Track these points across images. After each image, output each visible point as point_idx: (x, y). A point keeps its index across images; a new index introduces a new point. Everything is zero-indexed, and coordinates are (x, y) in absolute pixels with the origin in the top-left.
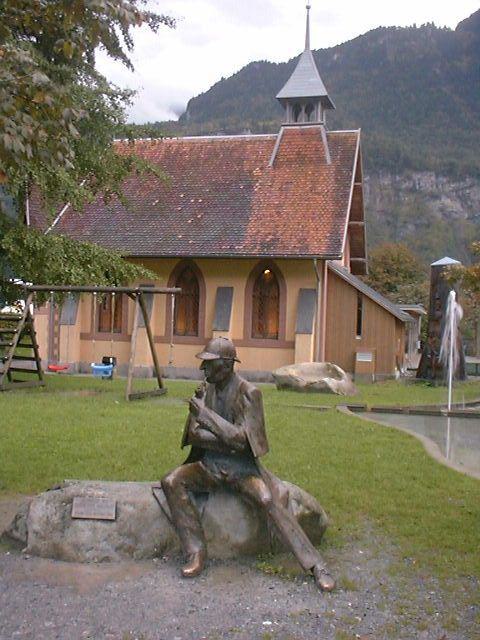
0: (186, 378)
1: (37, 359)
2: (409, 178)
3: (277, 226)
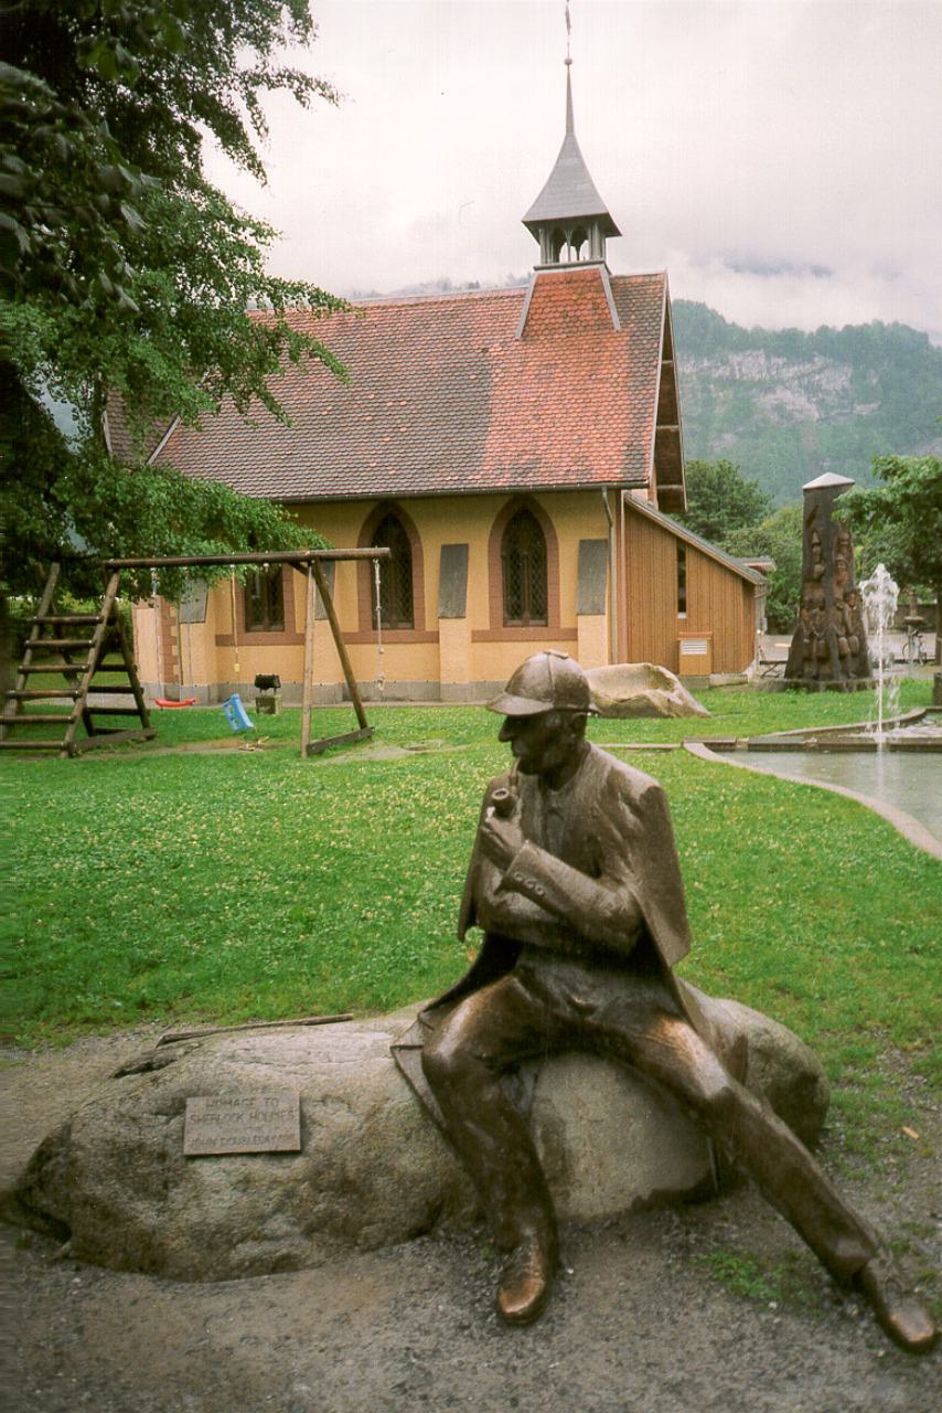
0: (399, 700)
1: (135, 690)
2: (725, 363)
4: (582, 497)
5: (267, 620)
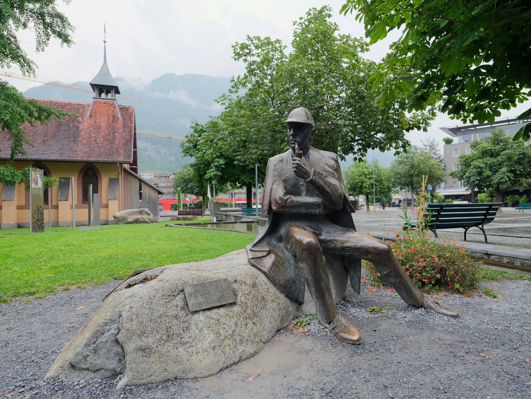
4: (111, 165)
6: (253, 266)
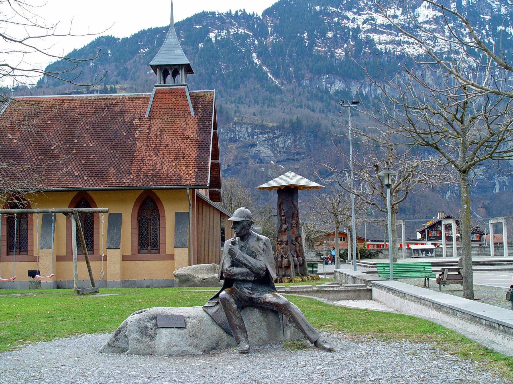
3: (156, 164)
5: (149, 248)
6: (205, 311)
